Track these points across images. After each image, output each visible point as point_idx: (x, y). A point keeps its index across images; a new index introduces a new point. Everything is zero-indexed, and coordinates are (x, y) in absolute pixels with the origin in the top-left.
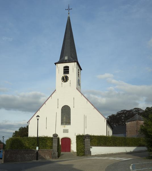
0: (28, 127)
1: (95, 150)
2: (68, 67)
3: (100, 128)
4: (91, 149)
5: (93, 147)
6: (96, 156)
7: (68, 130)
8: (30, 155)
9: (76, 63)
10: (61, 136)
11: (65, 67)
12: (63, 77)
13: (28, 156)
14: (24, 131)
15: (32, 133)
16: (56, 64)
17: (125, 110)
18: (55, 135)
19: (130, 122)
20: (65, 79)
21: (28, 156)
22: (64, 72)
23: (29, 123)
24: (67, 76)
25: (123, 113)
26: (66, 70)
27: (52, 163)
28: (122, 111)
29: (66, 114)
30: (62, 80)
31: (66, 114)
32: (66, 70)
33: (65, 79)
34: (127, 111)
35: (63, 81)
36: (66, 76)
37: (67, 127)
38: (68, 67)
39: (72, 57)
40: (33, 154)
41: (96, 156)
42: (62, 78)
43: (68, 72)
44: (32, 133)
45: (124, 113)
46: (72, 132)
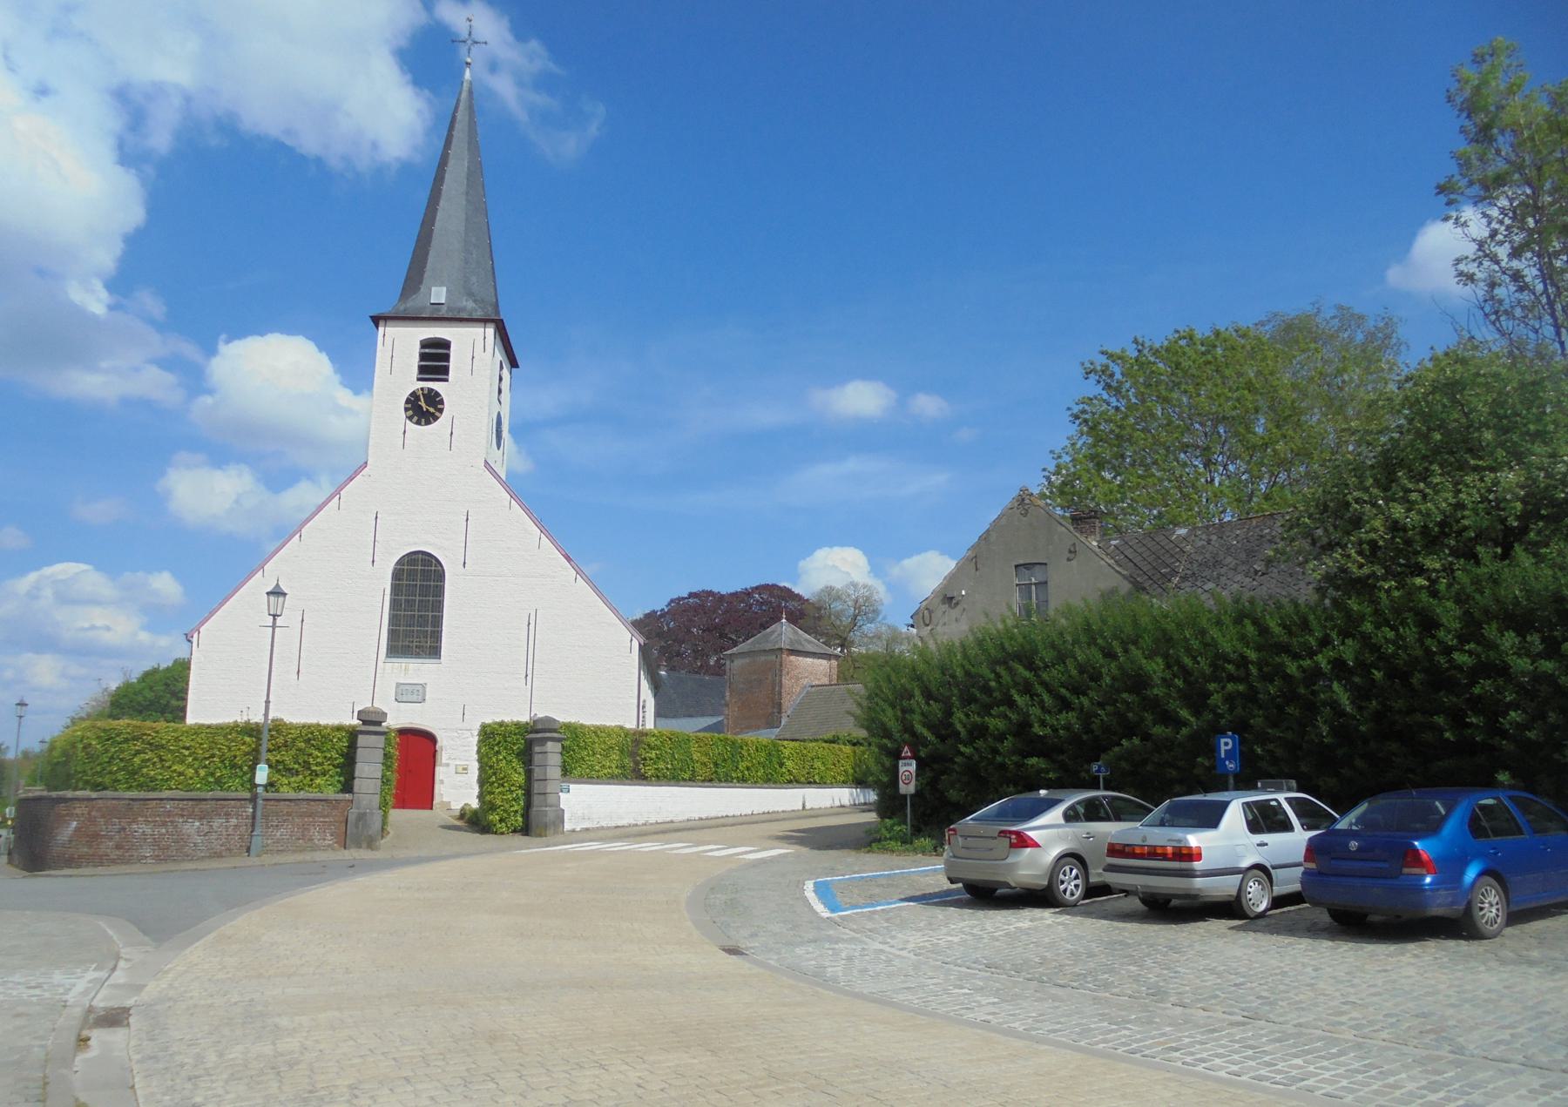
0: (183, 667)
1: (584, 803)
2: (446, 345)
3: (608, 686)
4: (475, 804)
5: (572, 786)
6: (587, 834)
7: (423, 686)
8: (217, 823)
9: (490, 331)
10: (398, 717)
11: (426, 344)
12: (413, 394)
13: (206, 828)
14: (163, 692)
15: (211, 704)
16: (377, 320)
17: (710, 593)
18: (372, 720)
19: (747, 660)
20: (424, 408)
21: (206, 828)
22: (422, 370)
23: (195, 640)
24: (437, 394)
25: (696, 609)
26: (435, 360)
27: (770, 837)
28: (691, 595)
29: (417, 603)
30: (406, 410)
31: (417, 603)
32: (435, 360)
33: (424, 408)
34: (721, 598)
35: (410, 418)
36: (430, 390)
37: (415, 670)
38: (446, 345)
39: (470, 294)
40: (234, 821)
41: (592, 835)
42: (408, 401)
43: (445, 370)
44: (211, 704)
45: (702, 606)
46: (456, 702)
